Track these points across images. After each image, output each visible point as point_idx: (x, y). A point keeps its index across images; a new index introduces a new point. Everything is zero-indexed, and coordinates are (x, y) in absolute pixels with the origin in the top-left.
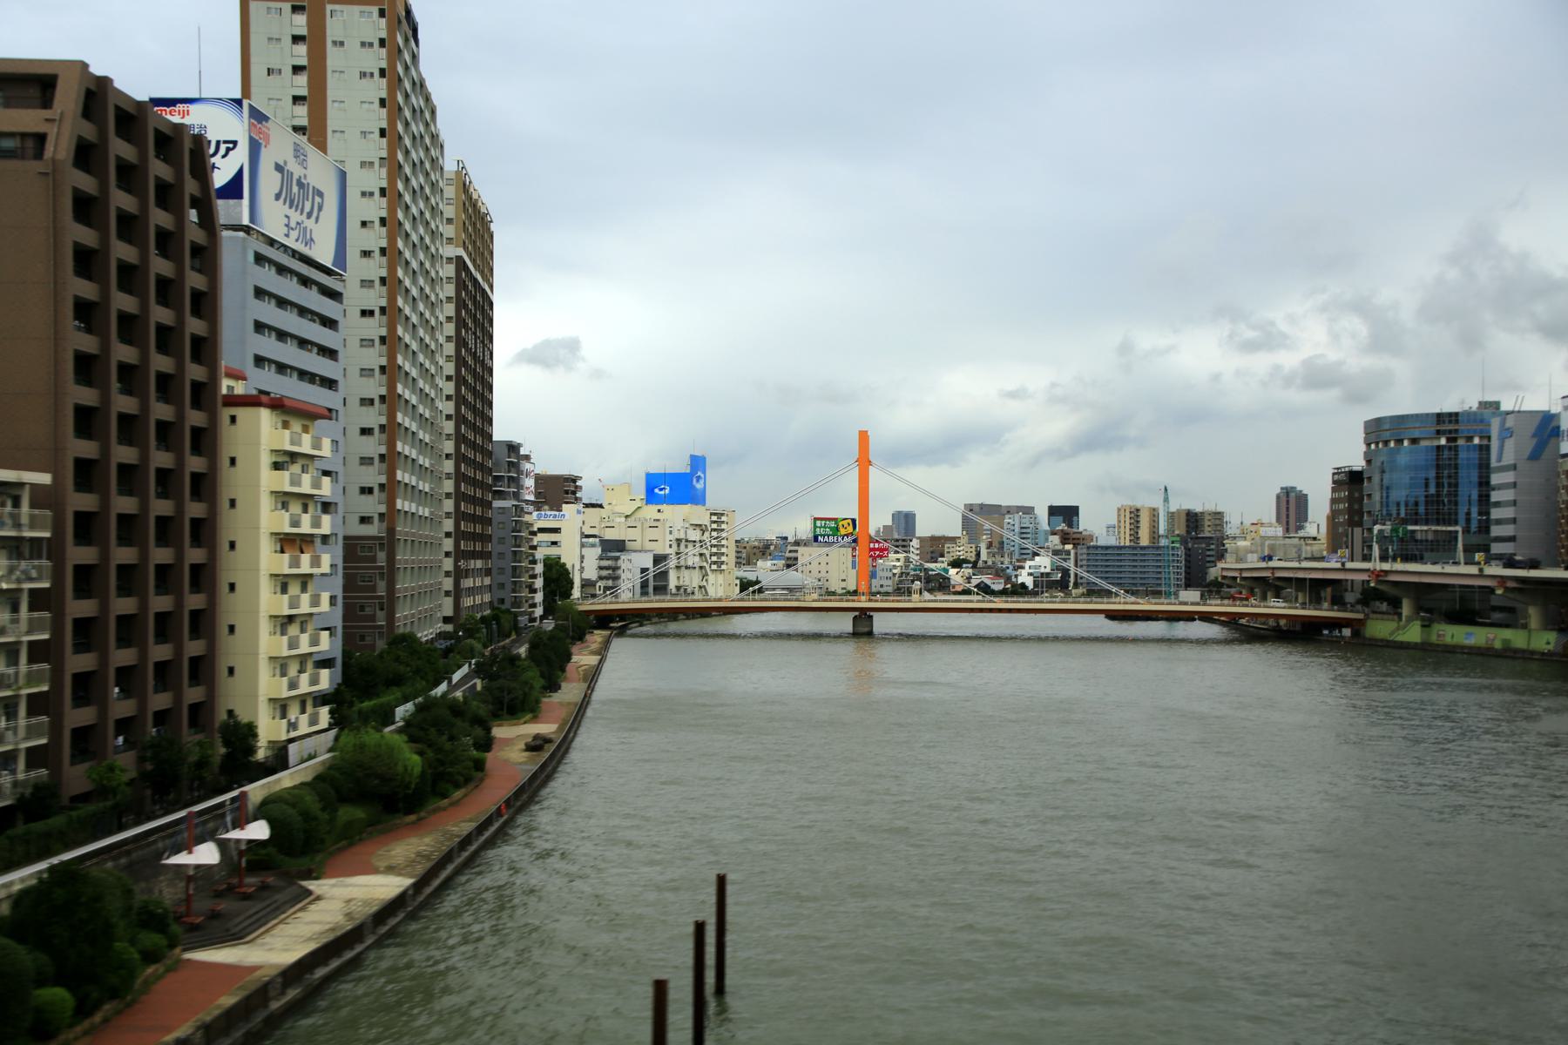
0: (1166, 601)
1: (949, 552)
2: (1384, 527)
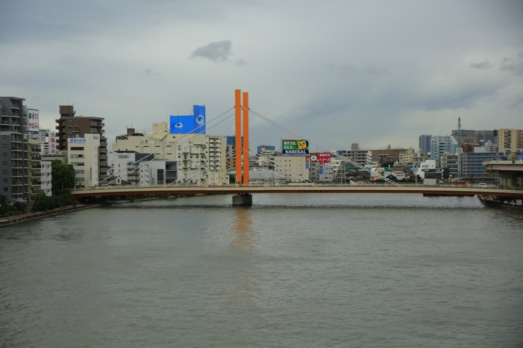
1: (401, 158)
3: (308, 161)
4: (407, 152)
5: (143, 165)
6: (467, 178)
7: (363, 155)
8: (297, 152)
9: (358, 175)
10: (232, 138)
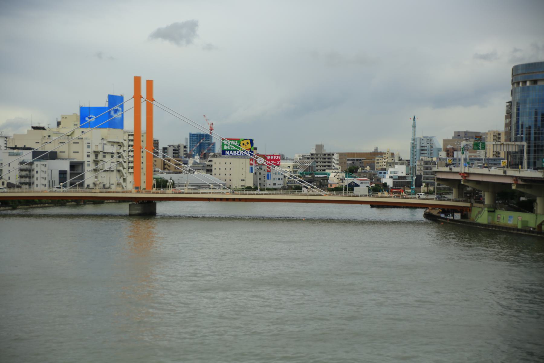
0: (80, 190)
1: (378, 163)
2: (468, 143)
3: (252, 164)
4: (384, 155)
5: (38, 166)
6: (446, 188)
7: (329, 159)
8: (240, 153)
10: (196, 136)
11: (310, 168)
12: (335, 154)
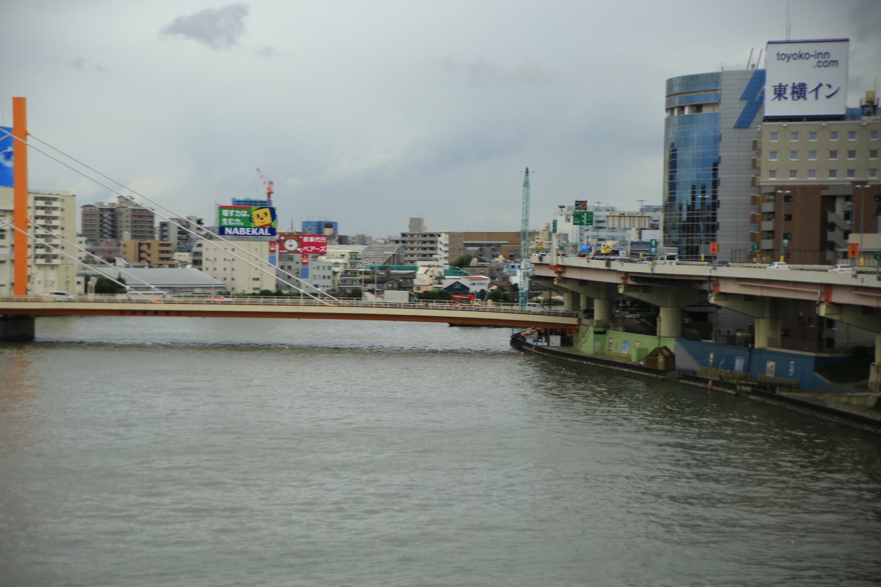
7: (432, 242)
9: (385, 282)
11: (394, 258)
12: (442, 234)
